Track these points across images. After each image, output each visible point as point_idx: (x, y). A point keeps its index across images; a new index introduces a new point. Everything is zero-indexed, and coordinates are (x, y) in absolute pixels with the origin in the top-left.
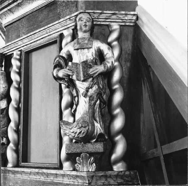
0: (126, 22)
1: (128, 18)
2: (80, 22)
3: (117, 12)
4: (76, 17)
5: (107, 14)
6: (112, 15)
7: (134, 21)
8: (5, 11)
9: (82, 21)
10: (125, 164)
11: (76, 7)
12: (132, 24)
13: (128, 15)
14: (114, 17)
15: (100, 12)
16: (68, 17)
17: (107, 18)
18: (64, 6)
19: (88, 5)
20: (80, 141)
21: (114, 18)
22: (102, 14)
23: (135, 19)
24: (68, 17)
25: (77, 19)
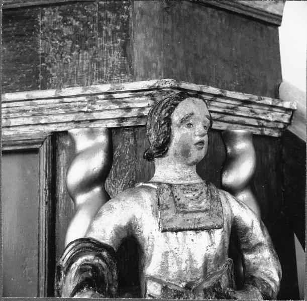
0: (265, 127)
1: (273, 116)
2: (185, 130)
3: (256, 97)
4: (171, 111)
5: (228, 101)
6: (240, 105)
7: (281, 126)
8: (168, 184)
9: (189, 125)
10: (240, 246)
11: (125, 54)
12: (276, 135)
13: (274, 109)
14: (243, 111)
15: (217, 91)
16: (105, 88)
17: (227, 111)
18: (68, 37)
19: (171, 58)
20: (33, 168)
21: (243, 114)
22: (218, 99)
23: (286, 121)
24: (105, 88)
25: (176, 118)
